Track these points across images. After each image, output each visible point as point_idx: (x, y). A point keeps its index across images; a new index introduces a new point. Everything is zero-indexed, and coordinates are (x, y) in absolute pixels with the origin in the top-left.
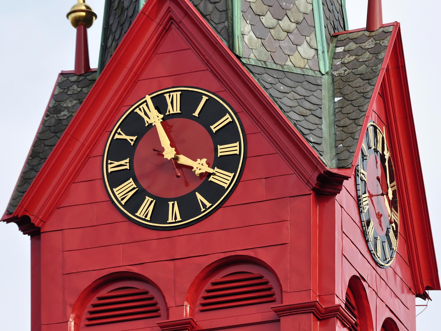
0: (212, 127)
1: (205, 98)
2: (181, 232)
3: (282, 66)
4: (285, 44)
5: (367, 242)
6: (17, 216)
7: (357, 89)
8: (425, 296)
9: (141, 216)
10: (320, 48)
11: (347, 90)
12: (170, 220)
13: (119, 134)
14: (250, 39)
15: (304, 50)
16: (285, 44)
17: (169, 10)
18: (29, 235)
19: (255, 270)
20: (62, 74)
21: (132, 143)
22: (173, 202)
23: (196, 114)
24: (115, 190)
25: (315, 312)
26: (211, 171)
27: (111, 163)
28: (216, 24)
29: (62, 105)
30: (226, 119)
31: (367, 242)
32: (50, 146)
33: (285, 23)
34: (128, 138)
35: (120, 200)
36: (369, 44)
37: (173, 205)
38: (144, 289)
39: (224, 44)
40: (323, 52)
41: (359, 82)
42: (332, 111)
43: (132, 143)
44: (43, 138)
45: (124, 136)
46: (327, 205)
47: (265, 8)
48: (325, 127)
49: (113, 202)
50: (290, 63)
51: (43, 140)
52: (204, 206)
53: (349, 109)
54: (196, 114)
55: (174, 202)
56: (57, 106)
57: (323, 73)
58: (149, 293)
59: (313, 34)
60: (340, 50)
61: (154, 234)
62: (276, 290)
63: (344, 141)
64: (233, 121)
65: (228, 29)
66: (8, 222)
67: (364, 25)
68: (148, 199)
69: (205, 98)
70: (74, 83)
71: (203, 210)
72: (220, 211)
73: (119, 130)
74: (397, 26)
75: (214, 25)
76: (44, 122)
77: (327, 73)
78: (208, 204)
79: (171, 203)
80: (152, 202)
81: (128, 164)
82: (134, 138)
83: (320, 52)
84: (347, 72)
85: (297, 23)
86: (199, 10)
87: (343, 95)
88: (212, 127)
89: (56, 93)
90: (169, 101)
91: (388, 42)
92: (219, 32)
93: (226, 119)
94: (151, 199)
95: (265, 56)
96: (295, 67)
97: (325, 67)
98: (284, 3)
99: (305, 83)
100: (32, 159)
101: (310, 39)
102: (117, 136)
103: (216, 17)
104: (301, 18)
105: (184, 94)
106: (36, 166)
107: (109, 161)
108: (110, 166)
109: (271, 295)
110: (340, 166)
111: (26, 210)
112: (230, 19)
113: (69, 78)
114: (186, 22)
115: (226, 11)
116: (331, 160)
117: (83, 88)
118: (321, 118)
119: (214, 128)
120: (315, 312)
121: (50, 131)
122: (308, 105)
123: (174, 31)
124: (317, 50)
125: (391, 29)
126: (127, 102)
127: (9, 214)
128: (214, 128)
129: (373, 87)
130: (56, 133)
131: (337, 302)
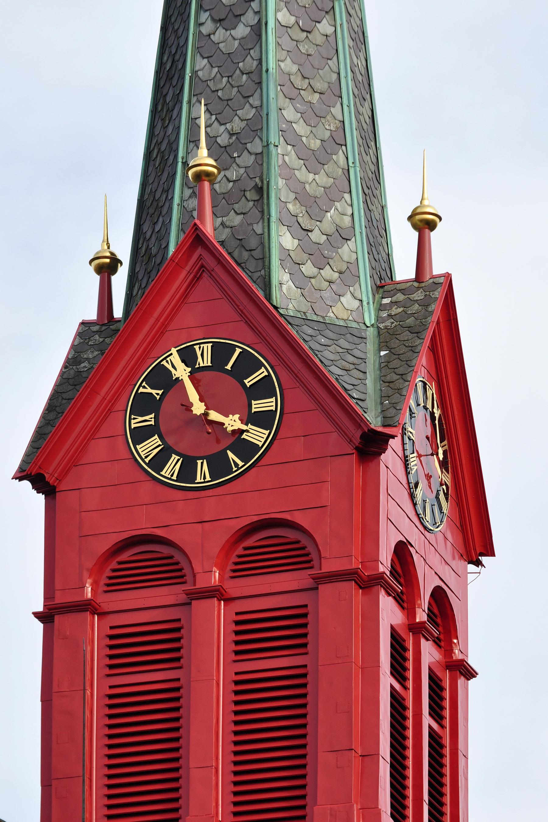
1: (238, 351)
2: (210, 492)
5: (415, 505)
6: (31, 473)
7: (405, 343)
8: (478, 563)
10: (365, 299)
11: (394, 343)
14: (289, 289)
16: (326, 294)
17: (200, 258)
19: (291, 535)
21: (158, 397)
22: (202, 461)
23: (229, 367)
25: (356, 579)
26: (244, 427)
27: (134, 419)
30: (262, 373)
31: (415, 505)
33: (327, 272)
34: (154, 392)
36: (418, 296)
37: (202, 463)
39: (261, 294)
41: (406, 335)
43: (158, 397)
46: (372, 465)
47: (306, 256)
48: (369, 382)
49: (136, 460)
52: (236, 465)
53: (396, 363)
54: (229, 367)
55: (162, 445)
59: (357, 285)
60: (386, 301)
61: (181, 495)
62: (314, 555)
64: (269, 375)
65: (265, 278)
68: (174, 457)
69: (238, 351)
71: (235, 469)
74: (448, 277)
75: (250, 274)
76: (62, 374)
77: (372, 325)
78: (241, 463)
79: (199, 462)
81: (153, 420)
82: (160, 392)
83: (365, 303)
84: (394, 325)
85: (340, 273)
86: (233, 258)
87: (388, 348)
90: (199, 353)
91: (439, 294)
93: (262, 373)
94: (177, 457)
95: (305, 306)
96: (337, 318)
97: (370, 318)
101: (354, 290)
102: (141, 390)
103: (252, 265)
108: (133, 421)
109: (309, 561)
110: (386, 424)
111: (40, 468)
114: (219, 271)
117: (106, 338)
119: (248, 382)
120: (356, 579)
122: (351, 359)
123: (206, 280)
125: (442, 280)
126: (154, 354)
128: (248, 382)
129: (422, 341)
131: (381, 569)
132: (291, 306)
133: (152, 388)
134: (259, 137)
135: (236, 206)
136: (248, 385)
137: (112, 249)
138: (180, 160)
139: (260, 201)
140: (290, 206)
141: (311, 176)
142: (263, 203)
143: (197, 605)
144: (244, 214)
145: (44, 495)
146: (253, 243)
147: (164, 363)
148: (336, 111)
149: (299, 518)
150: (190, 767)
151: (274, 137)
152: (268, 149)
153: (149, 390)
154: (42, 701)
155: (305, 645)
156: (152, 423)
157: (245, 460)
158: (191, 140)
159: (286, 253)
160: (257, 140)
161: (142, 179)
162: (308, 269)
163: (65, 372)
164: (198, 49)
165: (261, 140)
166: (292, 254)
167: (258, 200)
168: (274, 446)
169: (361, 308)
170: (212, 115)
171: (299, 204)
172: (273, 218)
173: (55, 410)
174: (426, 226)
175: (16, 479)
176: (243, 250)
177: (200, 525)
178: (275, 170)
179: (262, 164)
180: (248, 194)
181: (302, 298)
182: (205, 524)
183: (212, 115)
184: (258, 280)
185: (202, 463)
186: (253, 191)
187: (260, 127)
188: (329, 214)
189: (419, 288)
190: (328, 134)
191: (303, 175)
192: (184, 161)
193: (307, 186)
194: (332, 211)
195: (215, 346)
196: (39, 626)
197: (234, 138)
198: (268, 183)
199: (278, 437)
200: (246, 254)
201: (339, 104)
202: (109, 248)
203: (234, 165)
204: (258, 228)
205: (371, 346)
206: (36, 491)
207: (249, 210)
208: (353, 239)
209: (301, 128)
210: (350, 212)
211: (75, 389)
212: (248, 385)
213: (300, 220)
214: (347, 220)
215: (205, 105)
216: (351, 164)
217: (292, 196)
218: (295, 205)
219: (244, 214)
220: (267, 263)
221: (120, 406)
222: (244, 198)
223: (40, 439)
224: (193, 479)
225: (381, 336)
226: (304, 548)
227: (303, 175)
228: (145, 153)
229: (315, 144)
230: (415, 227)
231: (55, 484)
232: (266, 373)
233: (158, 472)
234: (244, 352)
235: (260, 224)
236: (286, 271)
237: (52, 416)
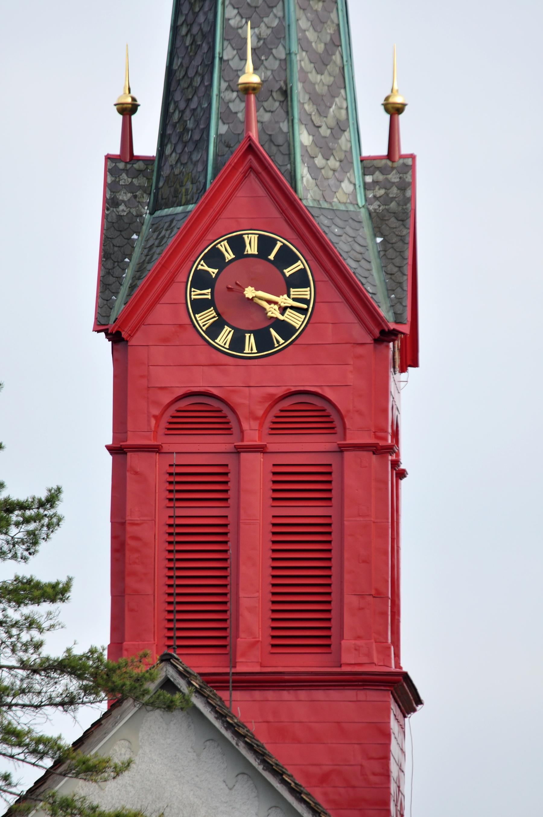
0: (285, 271)
1: (279, 245)
2: (256, 362)
3: (331, 203)
4: (332, 182)
6: (113, 332)
7: (394, 230)
9: (220, 343)
10: (357, 183)
12: (246, 351)
13: (202, 265)
14: (308, 181)
15: (346, 186)
18: (109, 341)
19: (319, 403)
20: (109, 158)
21: (214, 276)
23: (271, 257)
24: (197, 316)
27: (194, 291)
28: (280, 165)
29: (118, 197)
30: (298, 266)
32: (119, 247)
34: (211, 270)
35: (202, 326)
37: (250, 337)
38: (219, 408)
40: (360, 186)
41: (393, 222)
42: (376, 253)
43: (214, 276)
44: (110, 237)
45: (206, 268)
47: (317, 149)
48: (374, 272)
49: (195, 326)
50: (335, 200)
51: (111, 238)
52: (278, 342)
54: (271, 257)
56: (113, 197)
57: (361, 206)
58: (222, 411)
59: (351, 172)
63: (395, 291)
65: (291, 173)
66: (98, 332)
67: (385, 152)
68: (227, 329)
69: (279, 245)
70: (123, 171)
71: (276, 345)
72: (291, 347)
73: (202, 262)
74: (413, 157)
75: (278, 167)
77: (363, 206)
78: (281, 341)
79: (247, 335)
80: (230, 331)
81: (210, 294)
82: (216, 271)
83: (357, 186)
84: (381, 208)
85: (341, 161)
86: (265, 150)
87: (382, 235)
88: (285, 271)
89: (109, 181)
92: (283, 172)
93: (298, 266)
94: (229, 329)
96: (340, 202)
97: (361, 201)
98: (331, 144)
99: (350, 221)
100: (106, 260)
101: (350, 175)
102: (200, 267)
103: (280, 159)
104: (343, 157)
105: (261, 238)
106: (111, 269)
107: (193, 289)
108: (193, 293)
109: (333, 428)
110: (398, 321)
111: (119, 327)
112: (293, 163)
113: (117, 164)
115: (289, 154)
116: (388, 312)
117: (133, 178)
118: (370, 262)
121: (114, 228)
122: (358, 248)
124: (355, 185)
125: (409, 162)
126: (210, 237)
127: (98, 325)
128: (288, 272)
129: (408, 231)
130: (121, 231)
132: (309, 196)
133: (209, 267)
134: (282, 44)
135: (265, 104)
136: (288, 275)
137: (133, 93)
138: (217, 55)
139: (285, 103)
140: (306, 107)
141: (319, 77)
142: (287, 106)
143: (244, 456)
144: (272, 112)
145: (111, 342)
146: (280, 140)
147: (219, 246)
148: (333, 15)
149: (328, 393)
150: (240, 596)
151: (295, 48)
152: (290, 58)
153: (206, 268)
154: (111, 522)
155: (330, 499)
156: (209, 297)
157: (286, 339)
158: (226, 38)
159: (303, 147)
160: (281, 47)
161: (170, 48)
162: (319, 161)
163: (108, 215)
164: (221, 118)
165: (284, 47)
166: (309, 150)
167: (283, 102)
168: (307, 329)
169: (355, 191)
170: (242, 18)
171: (311, 104)
172: (296, 121)
173: (110, 257)
174: (397, 112)
175: (95, 331)
176: (272, 144)
177: (247, 388)
178: (296, 75)
179: (286, 69)
180: (274, 94)
181: (316, 188)
182: (252, 389)
183: (242, 18)
184: (285, 173)
185: (250, 337)
186: (278, 92)
187: (283, 36)
188: (331, 110)
189: (393, 168)
190: (328, 38)
191: (314, 77)
192: (221, 56)
193: (317, 87)
194: (334, 106)
195: (260, 237)
196: (108, 458)
197: (262, 42)
198: (291, 88)
199: (310, 322)
200: (274, 149)
201: (335, 10)
202: (129, 92)
203: (262, 67)
204: (284, 126)
205: (367, 230)
206: (111, 342)
207: (277, 109)
208: (348, 130)
209: (311, 35)
210: (345, 106)
211: (129, 243)
212: (288, 275)
213: (313, 118)
214: (343, 112)
215: (251, 28)
216: (345, 63)
217: (307, 97)
218: (309, 105)
219: (272, 112)
220: (292, 159)
221: (181, 277)
222: (271, 98)
223: (106, 290)
224: (242, 350)
225: (373, 220)
226: (328, 416)
227: (314, 77)
228: (172, 25)
229: (320, 48)
230: (387, 110)
231: (128, 340)
233: (214, 339)
234: (284, 247)
235: (286, 122)
236: (306, 165)
237: (109, 264)
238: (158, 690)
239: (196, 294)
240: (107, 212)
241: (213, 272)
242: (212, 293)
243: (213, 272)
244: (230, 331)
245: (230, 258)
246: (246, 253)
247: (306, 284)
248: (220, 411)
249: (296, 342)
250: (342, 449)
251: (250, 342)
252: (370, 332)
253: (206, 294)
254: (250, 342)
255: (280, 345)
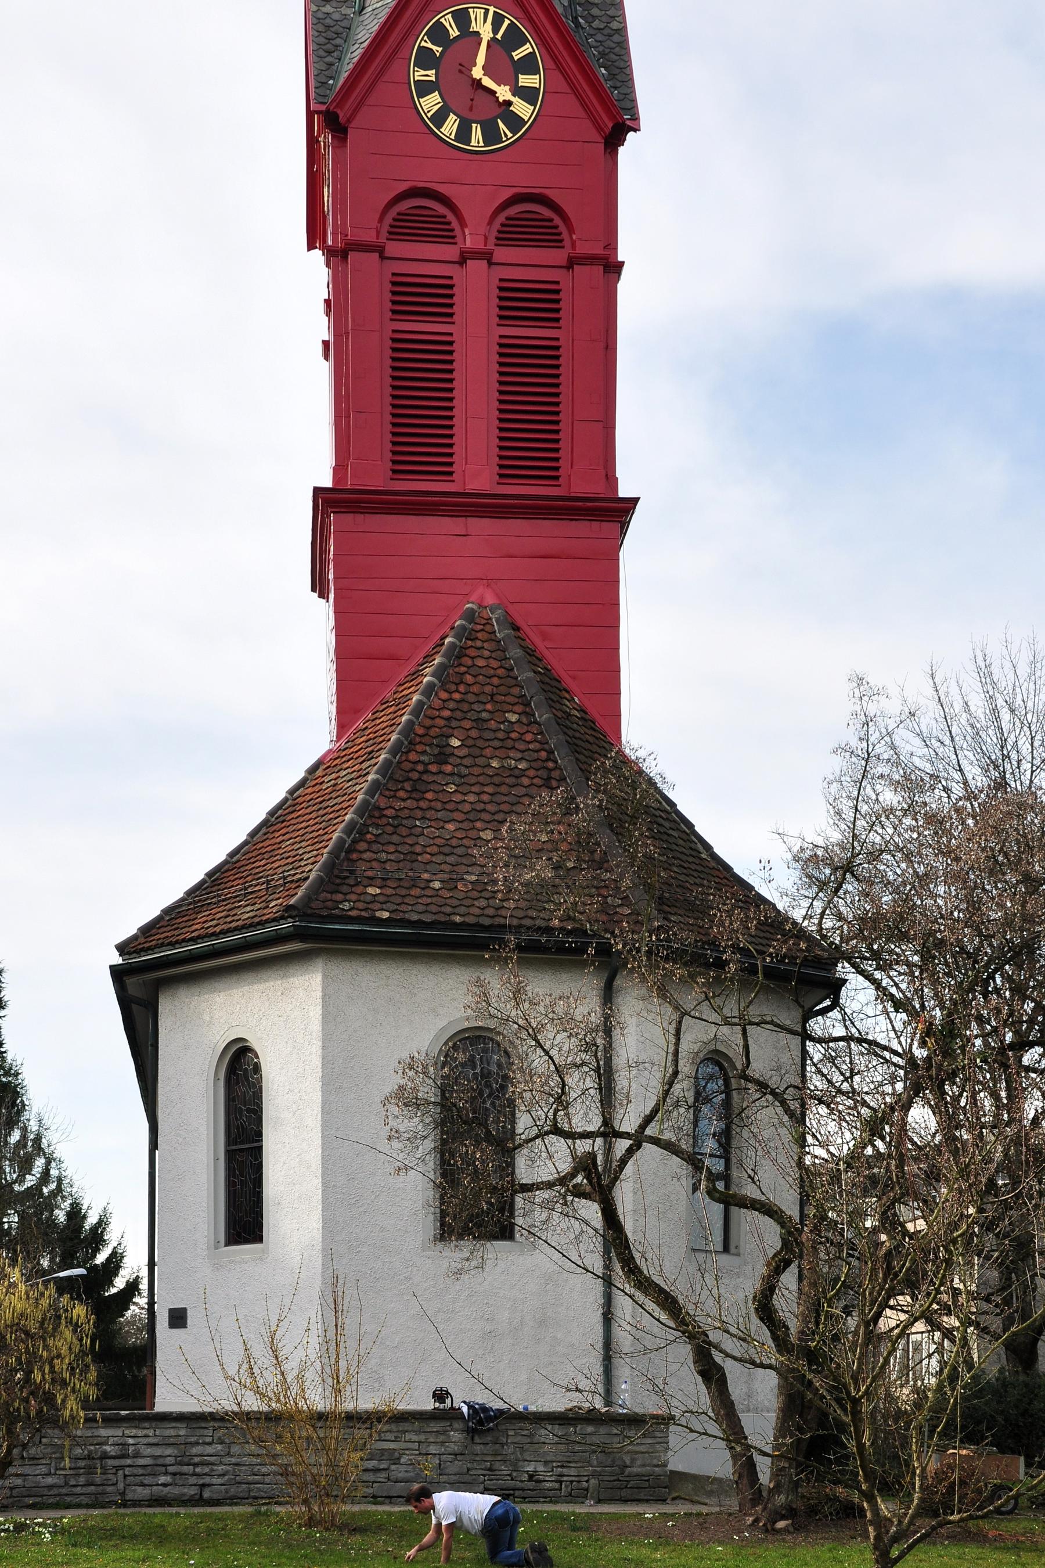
0: (514, 54)
1: (507, 22)
13: (425, 41)
20: (317, 491)
30: (526, 49)
34: (434, 48)
45: (429, 45)
52: (506, 135)
68: (452, 117)
69: (507, 22)
71: (504, 139)
79: (474, 125)
80: (439, 103)
82: (440, 49)
88: (514, 54)
93: (526, 49)
136: (516, 58)
153: (429, 45)
212: (516, 58)
232: (530, 50)
238: (403, 1497)
239: (419, 74)
240: (615, 25)
241: (437, 49)
242: (436, 74)
243: (437, 49)
244: (439, 103)
245: (455, 35)
246: (471, 30)
247: (439, 25)
248: (445, 217)
249: (527, 136)
250: (571, 263)
251: (477, 134)
252: (599, 128)
253: (431, 75)
254: (477, 134)
255: (508, 139)
